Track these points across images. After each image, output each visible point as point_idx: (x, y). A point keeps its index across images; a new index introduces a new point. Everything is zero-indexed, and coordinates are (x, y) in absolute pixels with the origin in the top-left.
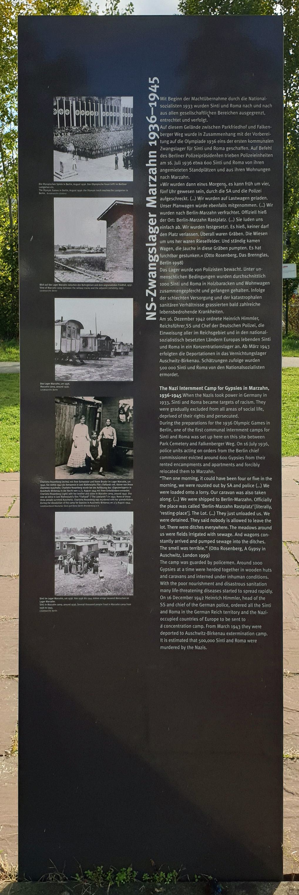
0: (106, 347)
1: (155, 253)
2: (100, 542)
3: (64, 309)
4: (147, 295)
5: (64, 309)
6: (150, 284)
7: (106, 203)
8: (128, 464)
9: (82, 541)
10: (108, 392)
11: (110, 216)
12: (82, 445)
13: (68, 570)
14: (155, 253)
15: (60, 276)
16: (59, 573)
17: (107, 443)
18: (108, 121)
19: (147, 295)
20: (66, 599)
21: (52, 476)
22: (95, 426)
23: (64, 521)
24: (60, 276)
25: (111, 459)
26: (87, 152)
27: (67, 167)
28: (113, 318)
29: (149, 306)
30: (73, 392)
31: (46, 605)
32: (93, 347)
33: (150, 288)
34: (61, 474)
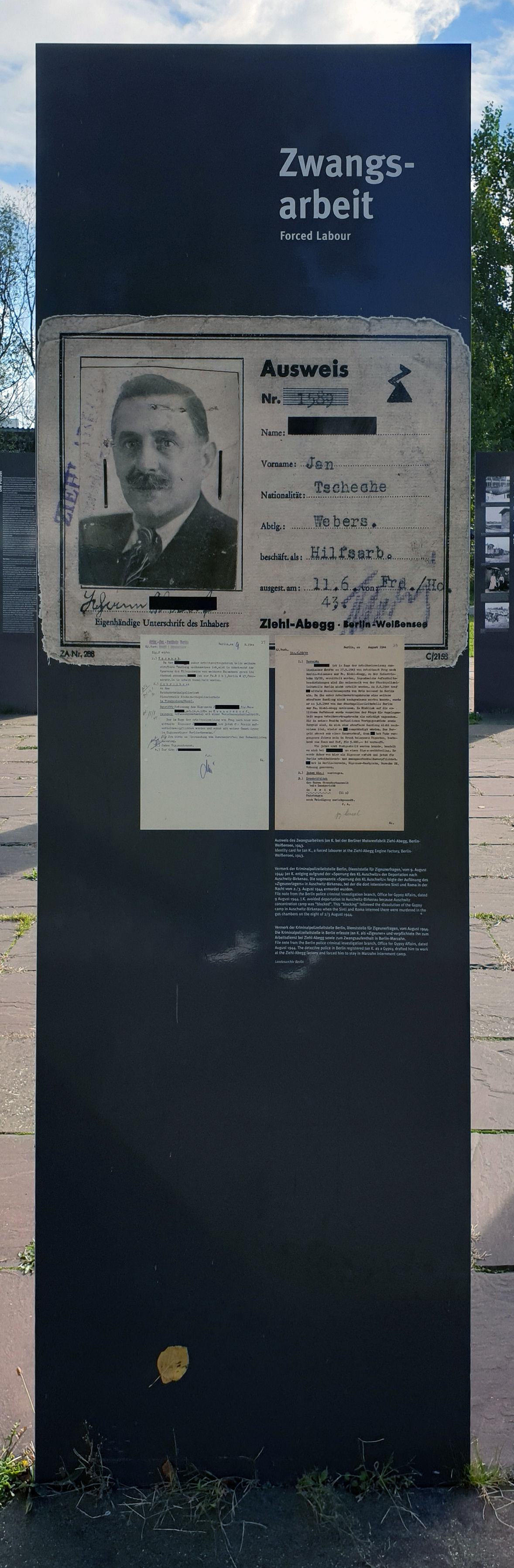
0: (501, 552)
1: (389, 174)
2: (499, 612)
3: (489, 541)
4: (283, 151)
5: (489, 541)
6: (311, 158)
7: (502, 508)
8: (507, 588)
9: (494, 612)
10: (502, 566)
11: (503, 512)
12: (493, 582)
13: (489, 620)
14: (389, 174)
15: (487, 531)
16: (486, 621)
17: (501, 582)
18: (502, 484)
19: (283, 151)
20: (488, 629)
21: (484, 592)
22: (497, 576)
23: (488, 606)
24: (487, 531)
25: (502, 587)
26: (496, 493)
27: (490, 498)
28: (504, 543)
29: (395, 161)
30: (490, 566)
31: (482, 631)
32: (497, 552)
33: (301, 158)
34: (487, 591)
